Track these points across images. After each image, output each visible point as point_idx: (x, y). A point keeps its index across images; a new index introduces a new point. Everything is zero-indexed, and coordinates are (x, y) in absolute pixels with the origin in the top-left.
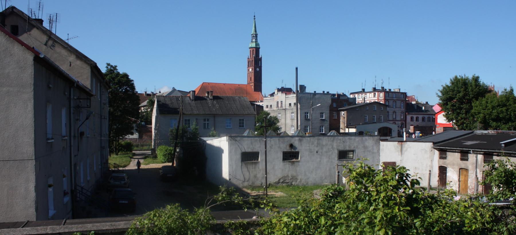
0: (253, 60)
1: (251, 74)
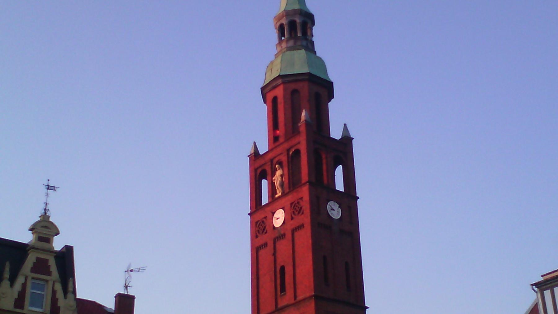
0: (303, 148)
1: (284, 247)
